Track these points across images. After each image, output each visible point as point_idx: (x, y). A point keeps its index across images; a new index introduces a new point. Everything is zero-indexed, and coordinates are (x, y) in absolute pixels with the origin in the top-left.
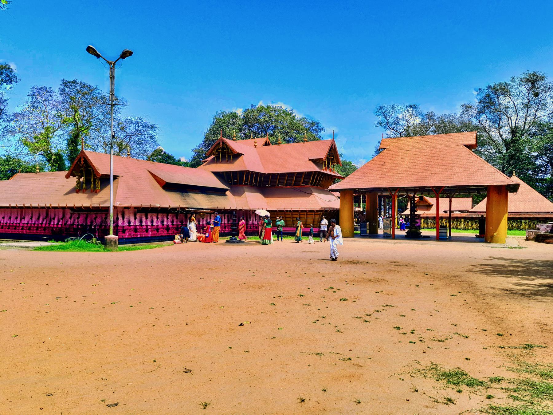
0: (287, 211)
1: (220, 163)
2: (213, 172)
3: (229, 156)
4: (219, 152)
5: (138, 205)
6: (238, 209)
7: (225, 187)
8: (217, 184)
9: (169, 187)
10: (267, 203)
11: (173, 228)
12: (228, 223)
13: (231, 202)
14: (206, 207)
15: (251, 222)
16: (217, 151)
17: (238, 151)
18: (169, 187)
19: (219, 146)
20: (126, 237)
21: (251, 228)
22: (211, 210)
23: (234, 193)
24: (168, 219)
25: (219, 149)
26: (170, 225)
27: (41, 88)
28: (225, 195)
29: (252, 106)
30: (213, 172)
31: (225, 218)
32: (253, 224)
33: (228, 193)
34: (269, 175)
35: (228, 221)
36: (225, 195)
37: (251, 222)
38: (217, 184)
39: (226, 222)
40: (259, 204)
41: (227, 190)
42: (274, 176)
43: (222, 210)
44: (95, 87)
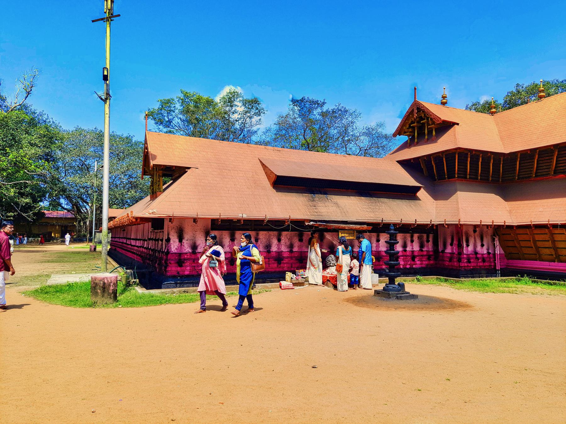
0: (555, 226)
1: (415, 146)
2: (398, 162)
3: (430, 132)
4: (413, 128)
5: (215, 215)
6: (435, 222)
7: (417, 184)
8: (405, 179)
9: (283, 184)
10: (510, 212)
11: (291, 258)
12: (421, 250)
13: (427, 210)
14: (354, 219)
15: (471, 248)
16: (410, 127)
17: (443, 117)
18: (283, 184)
19: (413, 115)
20: (187, 273)
21: (469, 262)
22: (368, 224)
23: (437, 194)
24: (279, 240)
25: (413, 122)
26: (278, 251)
27: (287, 116)
28: (417, 199)
29: (518, 85)
30: (398, 162)
31: (412, 241)
32: (476, 253)
33: (422, 194)
34: (513, 155)
35: (422, 246)
36: (417, 199)
37: (471, 248)
38: (405, 179)
39: (416, 247)
40: (476, 207)
41: (418, 189)
42: (527, 156)
43: (410, 225)
44: (322, 101)
